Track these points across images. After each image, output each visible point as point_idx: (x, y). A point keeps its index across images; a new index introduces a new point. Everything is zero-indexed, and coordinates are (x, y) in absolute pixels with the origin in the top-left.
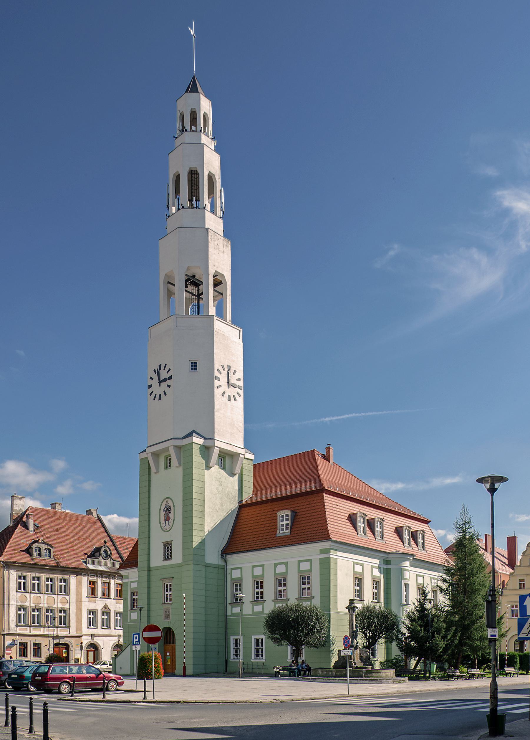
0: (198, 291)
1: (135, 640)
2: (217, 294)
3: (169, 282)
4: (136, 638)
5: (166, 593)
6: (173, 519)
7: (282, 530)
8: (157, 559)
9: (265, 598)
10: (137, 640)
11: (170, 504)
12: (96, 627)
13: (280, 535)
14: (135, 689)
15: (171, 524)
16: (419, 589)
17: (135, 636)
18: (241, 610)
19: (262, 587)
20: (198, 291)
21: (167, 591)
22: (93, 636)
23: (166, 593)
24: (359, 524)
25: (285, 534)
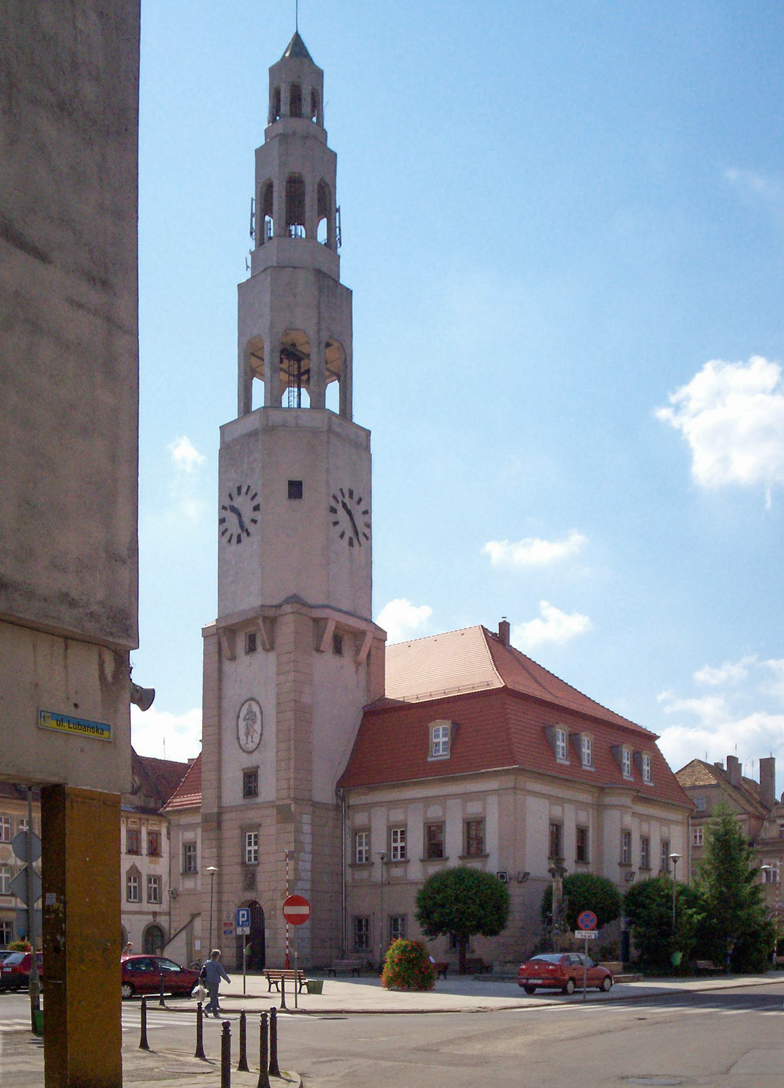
0: (299, 367)
1: (241, 919)
2: (258, 354)
3: (253, 354)
4: (243, 916)
5: (248, 848)
6: (259, 732)
7: (437, 751)
8: (233, 792)
9: (409, 854)
10: (245, 919)
11: (255, 708)
12: (140, 901)
13: (433, 759)
14: (242, 994)
15: (257, 740)
16: (662, 840)
17: (241, 912)
18: (370, 876)
19: (403, 839)
20: (299, 367)
21: (250, 844)
22: (155, 914)
23: (248, 848)
24: (446, 739)
25: (441, 758)
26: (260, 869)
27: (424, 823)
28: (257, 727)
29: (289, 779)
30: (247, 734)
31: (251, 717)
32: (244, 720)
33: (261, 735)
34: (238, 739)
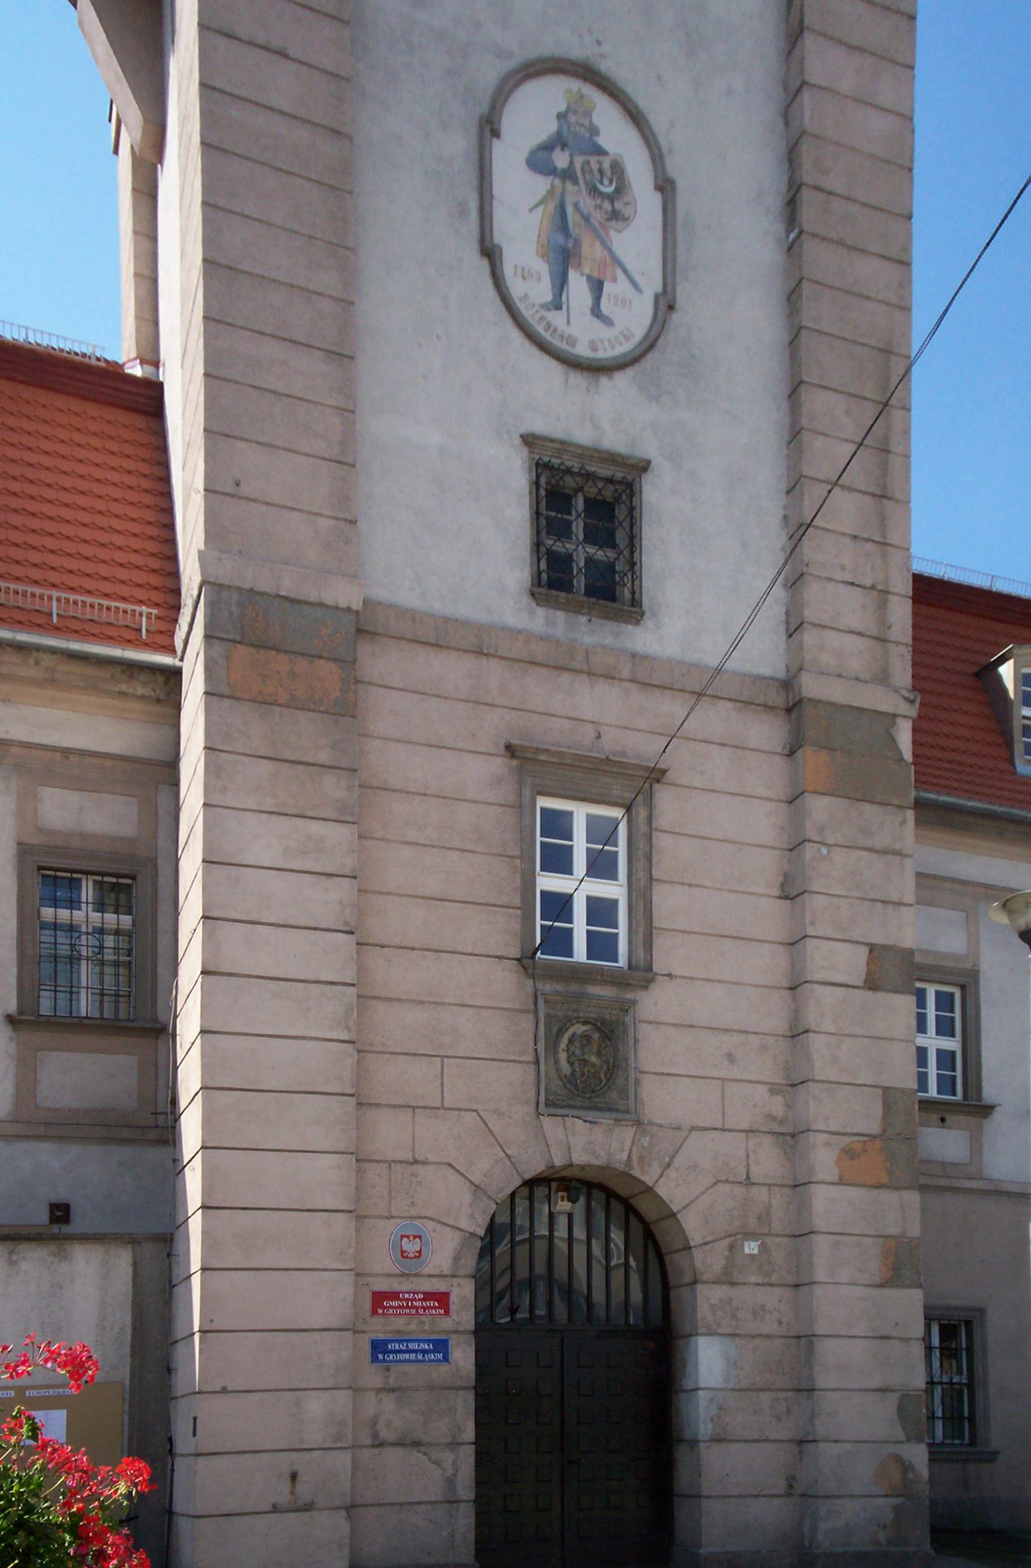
11: (615, 134)
15: (632, 316)
26: (655, 1003)
27: (23, 850)
28: (638, 243)
29: (883, 594)
30: (563, 257)
31: (568, 157)
32: (539, 161)
33: (666, 304)
34: (490, 253)
